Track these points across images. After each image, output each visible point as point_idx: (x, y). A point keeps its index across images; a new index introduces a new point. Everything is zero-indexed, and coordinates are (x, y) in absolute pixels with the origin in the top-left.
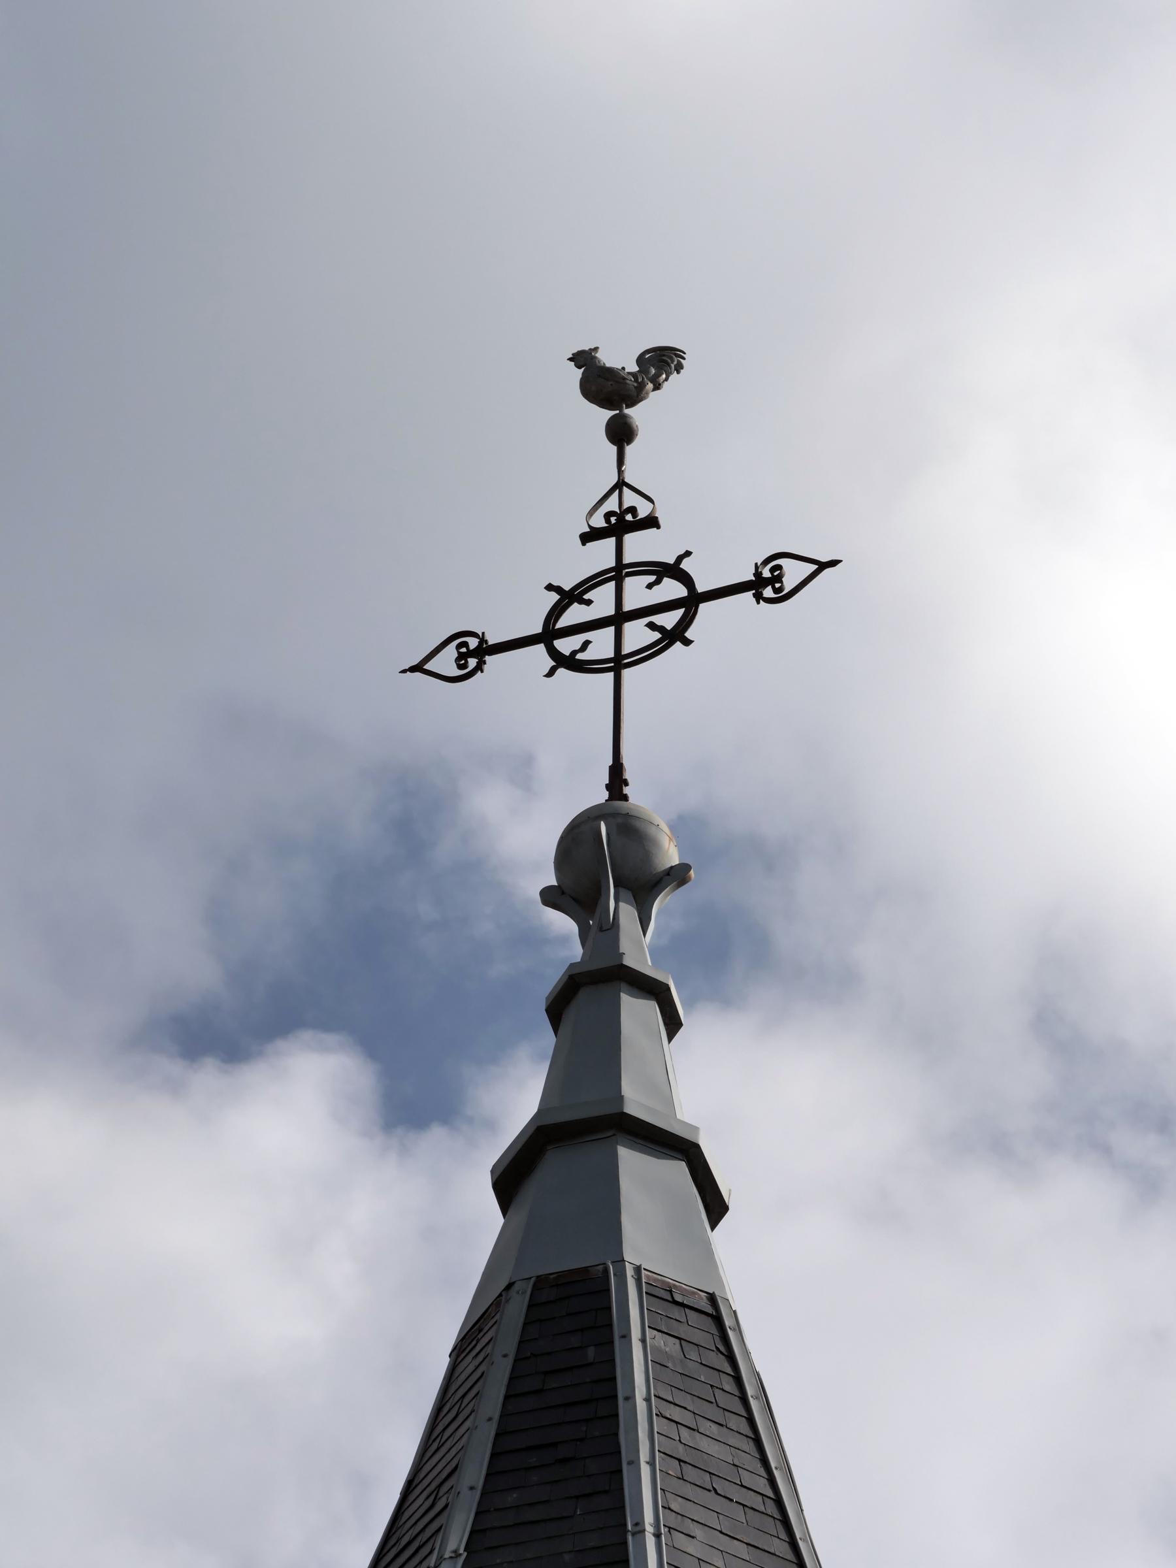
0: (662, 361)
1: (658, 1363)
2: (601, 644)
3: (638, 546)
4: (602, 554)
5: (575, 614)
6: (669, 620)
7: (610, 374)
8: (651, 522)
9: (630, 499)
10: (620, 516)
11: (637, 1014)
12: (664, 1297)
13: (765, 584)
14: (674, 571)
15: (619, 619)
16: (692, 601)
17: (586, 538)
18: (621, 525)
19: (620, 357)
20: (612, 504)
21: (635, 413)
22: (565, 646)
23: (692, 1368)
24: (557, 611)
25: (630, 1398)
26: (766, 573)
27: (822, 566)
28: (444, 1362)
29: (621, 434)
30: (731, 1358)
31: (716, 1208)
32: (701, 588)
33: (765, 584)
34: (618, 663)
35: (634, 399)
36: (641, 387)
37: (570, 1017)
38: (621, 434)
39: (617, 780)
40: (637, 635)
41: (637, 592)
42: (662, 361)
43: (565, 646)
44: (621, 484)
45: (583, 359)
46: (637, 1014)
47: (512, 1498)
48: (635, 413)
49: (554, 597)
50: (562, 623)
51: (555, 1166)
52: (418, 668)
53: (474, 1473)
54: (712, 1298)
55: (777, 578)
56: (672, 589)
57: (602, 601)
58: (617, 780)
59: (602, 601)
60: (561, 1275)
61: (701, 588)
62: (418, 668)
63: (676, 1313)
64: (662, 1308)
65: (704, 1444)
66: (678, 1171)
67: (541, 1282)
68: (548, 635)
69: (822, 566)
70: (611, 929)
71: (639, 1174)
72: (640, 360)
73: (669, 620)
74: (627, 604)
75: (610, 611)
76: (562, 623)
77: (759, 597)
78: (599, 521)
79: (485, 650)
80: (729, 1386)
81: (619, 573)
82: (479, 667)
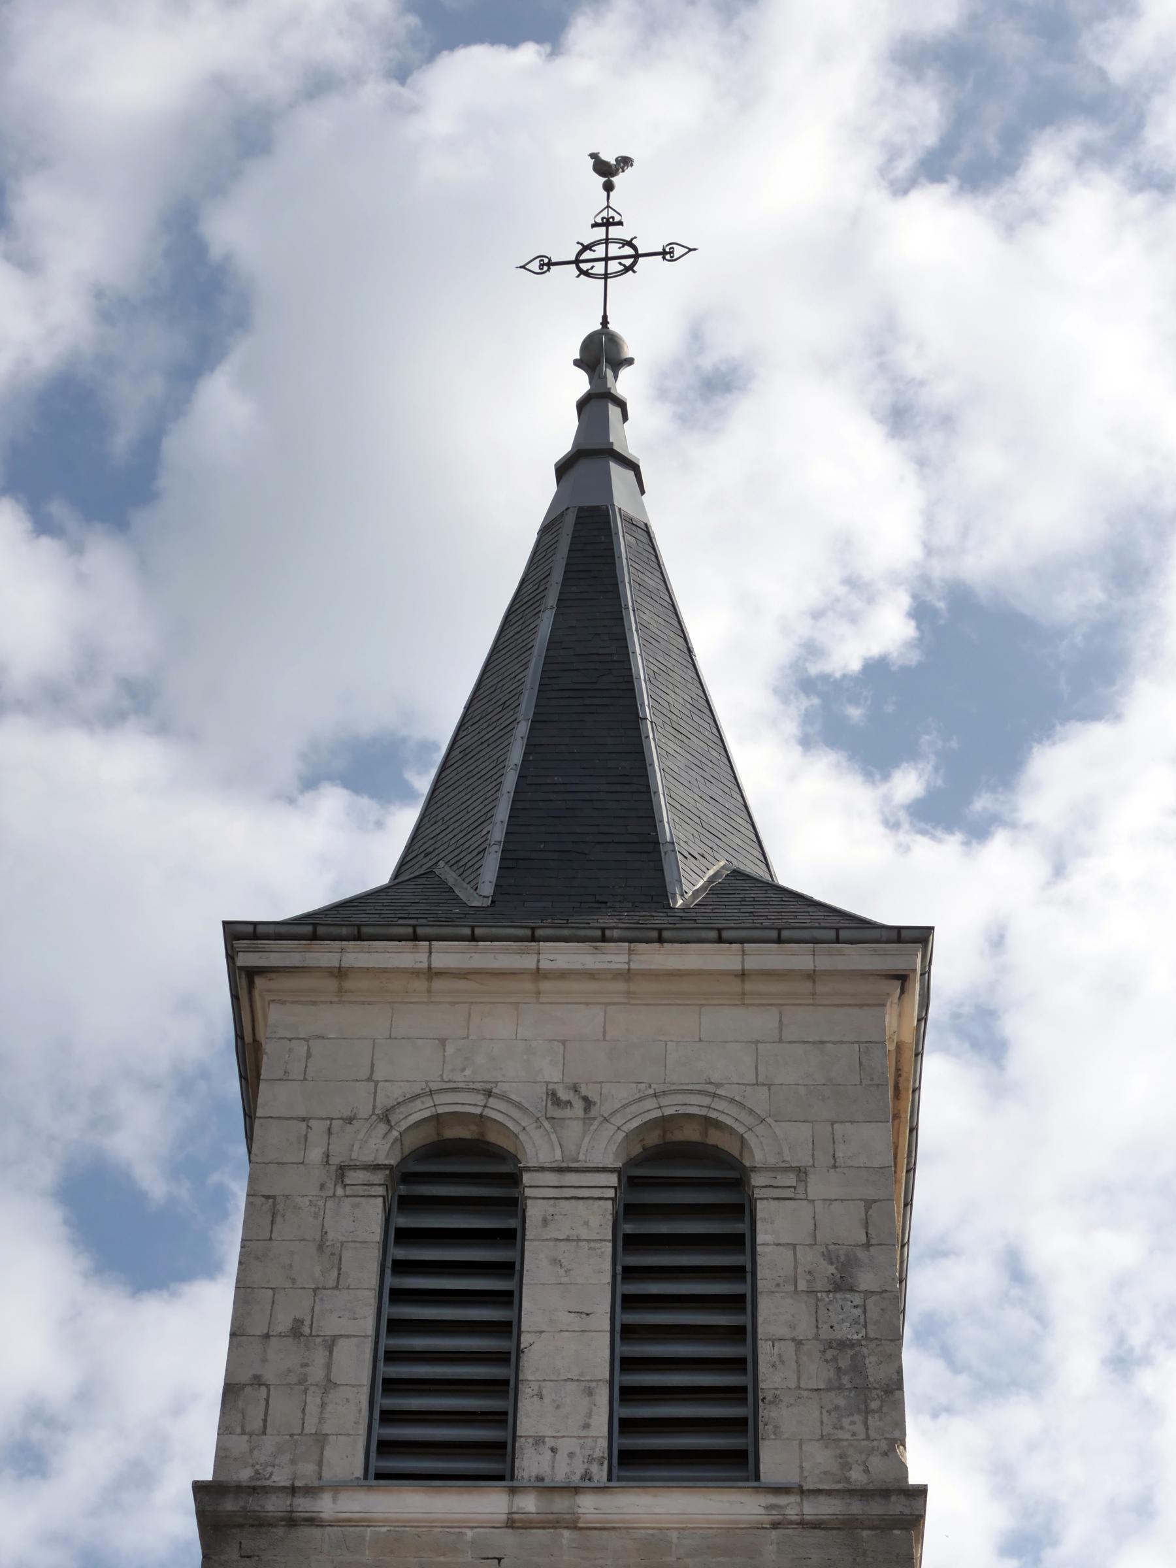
0: (625, 162)
1: (628, 546)
2: (599, 268)
3: (614, 232)
4: (600, 233)
5: (587, 255)
6: (628, 262)
7: (606, 164)
8: (620, 223)
9: (612, 213)
10: (608, 219)
11: (614, 412)
12: (630, 522)
13: (666, 254)
14: (630, 244)
15: (607, 259)
16: (637, 256)
17: (595, 225)
18: (607, 223)
19: (610, 157)
20: (604, 214)
21: (614, 179)
22: (584, 266)
23: (640, 550)
24: (581, 253)
25: (620, 557)
26: (667, 249)
27: (690, 250)
28: (535, 537)
29: (609, 187)
30: (654, 548)
31: (643, 492)
32: (640, 252)
33: (666, 254)
34: (606, 276)
35: (614, 174)
36: (617, 170)
37: (587, 409)
38: (609, 187)
39: (605, 321)
40: (614, 266)
41: (614, 250)
42: (625, 162)
43: (584, 266)
44: (608, 207)
45: (594, 156)
46: (614, 412)
47: (574, 589)
48: (614, 179)
49: (580, 247)
50: (582, 258)
51: (583, 466)
52: (523, 267)
53: (557, 576)
54: (646, 525)
55: (541, 265)
56: (628, 251)
57: (600, 251)
58: (605, 321)
59: (600, 251)
60: (588, 507)
61: (640, 252)
62: (523, 267)
63: (634, 528)
64: (630, 526)
65: (646, 579)
66: (631, 474)
67: (580, 509)
68: (577, 262)
69: (690, 250)
70: (604, 378)
71: (619, 476)
72: (616, 160)
73: (628, 262)
74: (608, 255)
75: (603, 256)
76: (582, 258)
77: (664, 258)
78: (599, 220)
79: (550, 264)
80: (654, 559)
81: (607, 241)
82: (549, 270)
